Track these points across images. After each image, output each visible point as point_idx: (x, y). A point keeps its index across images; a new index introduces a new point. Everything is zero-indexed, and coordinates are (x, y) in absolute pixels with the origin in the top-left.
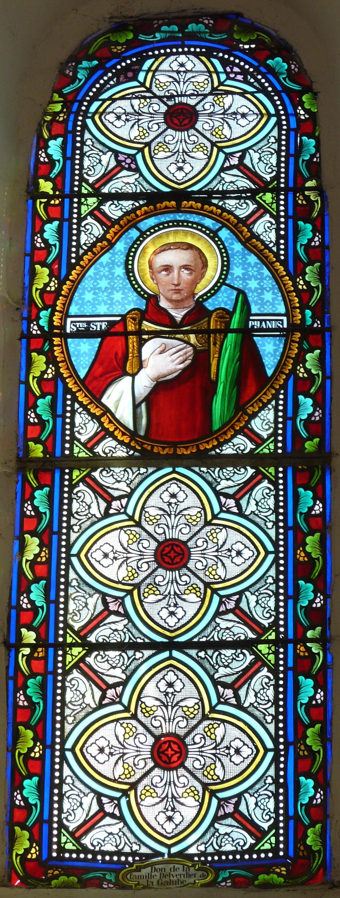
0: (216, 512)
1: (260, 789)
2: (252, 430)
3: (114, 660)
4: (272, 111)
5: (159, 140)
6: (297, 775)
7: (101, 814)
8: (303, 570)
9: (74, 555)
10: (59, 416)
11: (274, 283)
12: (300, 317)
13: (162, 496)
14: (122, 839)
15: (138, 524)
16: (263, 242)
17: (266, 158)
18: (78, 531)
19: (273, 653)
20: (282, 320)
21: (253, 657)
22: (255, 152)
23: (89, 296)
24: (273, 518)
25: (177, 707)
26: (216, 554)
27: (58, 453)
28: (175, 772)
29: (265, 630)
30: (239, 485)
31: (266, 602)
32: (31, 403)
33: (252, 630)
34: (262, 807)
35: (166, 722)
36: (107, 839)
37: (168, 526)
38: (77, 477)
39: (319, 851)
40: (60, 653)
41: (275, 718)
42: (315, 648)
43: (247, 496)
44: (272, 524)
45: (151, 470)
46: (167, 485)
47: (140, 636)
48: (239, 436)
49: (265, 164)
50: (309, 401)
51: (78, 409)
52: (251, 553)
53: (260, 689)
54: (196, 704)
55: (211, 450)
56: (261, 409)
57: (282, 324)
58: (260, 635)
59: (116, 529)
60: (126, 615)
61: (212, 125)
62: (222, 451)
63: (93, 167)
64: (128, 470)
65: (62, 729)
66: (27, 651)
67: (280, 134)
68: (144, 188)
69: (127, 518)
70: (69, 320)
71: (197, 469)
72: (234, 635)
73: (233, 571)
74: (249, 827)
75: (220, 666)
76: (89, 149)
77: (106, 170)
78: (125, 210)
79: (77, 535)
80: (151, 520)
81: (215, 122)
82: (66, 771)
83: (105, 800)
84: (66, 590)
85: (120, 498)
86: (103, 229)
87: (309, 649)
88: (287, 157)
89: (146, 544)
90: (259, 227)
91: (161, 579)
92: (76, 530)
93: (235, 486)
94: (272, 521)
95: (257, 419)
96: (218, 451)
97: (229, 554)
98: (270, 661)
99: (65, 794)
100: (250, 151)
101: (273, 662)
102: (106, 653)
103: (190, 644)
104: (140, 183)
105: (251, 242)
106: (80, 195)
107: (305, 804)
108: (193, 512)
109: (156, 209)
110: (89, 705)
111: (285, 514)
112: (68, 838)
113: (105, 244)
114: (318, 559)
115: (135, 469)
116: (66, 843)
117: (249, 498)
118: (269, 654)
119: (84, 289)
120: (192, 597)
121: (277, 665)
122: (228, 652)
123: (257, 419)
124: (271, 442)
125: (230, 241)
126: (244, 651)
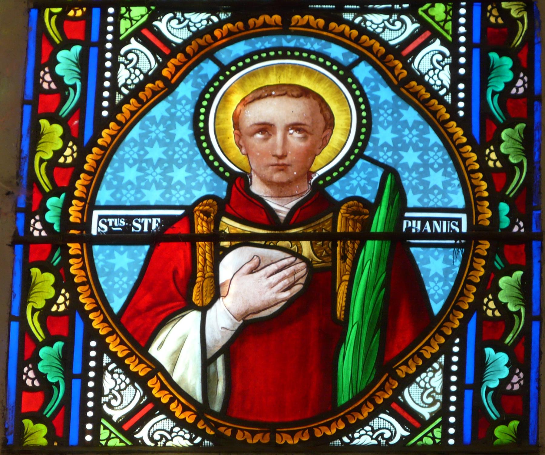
2: (405, 406)
10: (77, 377)
11: (447, 157)
16: (428, 87)
20: (459, 220)
23: (130, 174)
38: (127, 30)
48: (382, 415)
56: (421, 370)
62: (352, 439)
86: (157, 60)
90: (422, 62)
95: (414, 386)
102: (187, 15)
109: (247, 27)
124: (437, 426)
125: (373, 84)
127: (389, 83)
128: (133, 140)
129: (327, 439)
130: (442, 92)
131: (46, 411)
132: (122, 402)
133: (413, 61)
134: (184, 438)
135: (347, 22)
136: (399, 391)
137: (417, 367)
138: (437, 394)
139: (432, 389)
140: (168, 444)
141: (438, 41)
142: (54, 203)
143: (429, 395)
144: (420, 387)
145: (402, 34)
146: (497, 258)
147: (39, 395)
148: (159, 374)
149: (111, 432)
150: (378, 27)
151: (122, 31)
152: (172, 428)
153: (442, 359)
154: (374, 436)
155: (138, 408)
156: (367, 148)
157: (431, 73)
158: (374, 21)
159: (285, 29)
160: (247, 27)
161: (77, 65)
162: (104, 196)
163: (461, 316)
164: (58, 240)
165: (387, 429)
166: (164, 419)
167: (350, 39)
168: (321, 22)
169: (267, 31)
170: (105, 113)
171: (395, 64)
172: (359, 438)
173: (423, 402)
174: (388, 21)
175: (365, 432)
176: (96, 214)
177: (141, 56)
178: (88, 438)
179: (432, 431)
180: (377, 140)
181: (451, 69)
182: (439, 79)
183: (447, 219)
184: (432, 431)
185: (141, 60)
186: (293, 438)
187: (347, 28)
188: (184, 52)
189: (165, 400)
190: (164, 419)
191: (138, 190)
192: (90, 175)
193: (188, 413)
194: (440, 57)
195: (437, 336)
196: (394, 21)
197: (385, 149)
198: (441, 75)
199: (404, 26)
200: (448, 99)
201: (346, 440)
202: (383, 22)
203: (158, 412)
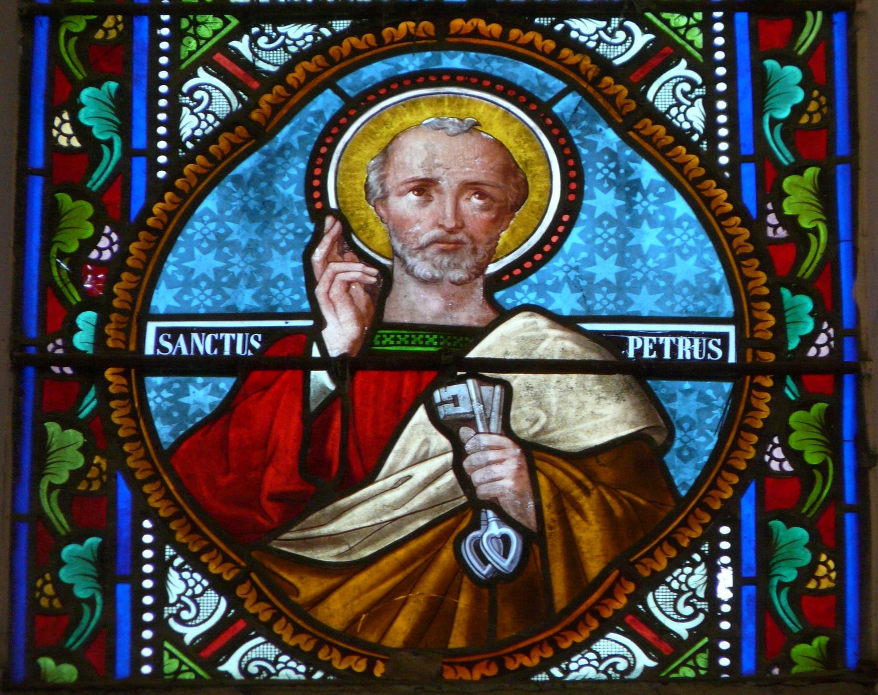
11: (703, 237)
12: (772, 320)
16: (672, 130)
19: (699, 24)
20: (724, 337)
21: (651, 36)
23: (205, 263)
32: (45, 552)
48: (611, 635)
50: (794, 73)
51: (173, 558)
56: (675, 564)
57: (725, 347)
62: (567, 672)
70: (151, 328)
86: (239, 99)
90: (661, 94)
95: (663, 588)
96: (556, 672)
98: (691, 43)
105: (640, 125)
107: (785, 121)
109: (380, 41)
113: (248, 130)
118: (688, 27)
119: (191, 244)
121: (709, 48)
123: (662, 592)
124: (702, 650)
125: (584, 255)
127: (611, 124)
129: (526, 673)
130: (178, 561)
131: (71, 641)
132: (197, 614)
133: (228, 611)
134: (578, 31)
135: (540, 29)
136: (248, 108)
137: (670, 560)
138: (700, 599)
139: (196, 111)
140: (603, 24)
142: (87, 319)
143: (199, 102)
144: (672, 590)
145: (627, 50)
148: (254, 576)
149: (182, 663)
150: (589, 40)
151: (184, 53)
152: (277, 657)
153: (705, 548)
154: (282, 37)
156: (577, 222)
157: (198, 590)
158: (583, 31)
159: (443, 42)
160: (380, 41)
163: (150, 221)
165: (263, 49)
166: (263, 643)
169: (411, 45)
171: (621, 96)
172: (305, 35)
173: (678, 613)
174: (605, 30)
175: (586, 662)
177: (215, 94)
178: (146, 669)
179: (693, 657)
180: (593, 209)
181: (705, 104)
182: (686, 120)
183: (699, 334)
184: (693, 657)
185: (211, 99)
186: (471, 671)
188: (602, 621)
189: (265, 617)
190: (263, 643)
192: (747, 425)
194: (687, 87)
195: (187, 190)
196: (614, 31)
197: (605, 223)
198: (181, 587)
199: (243, 666)
200: (169, 551)
201: (326, 32)
202: (597, 32)
203: (253, 633)
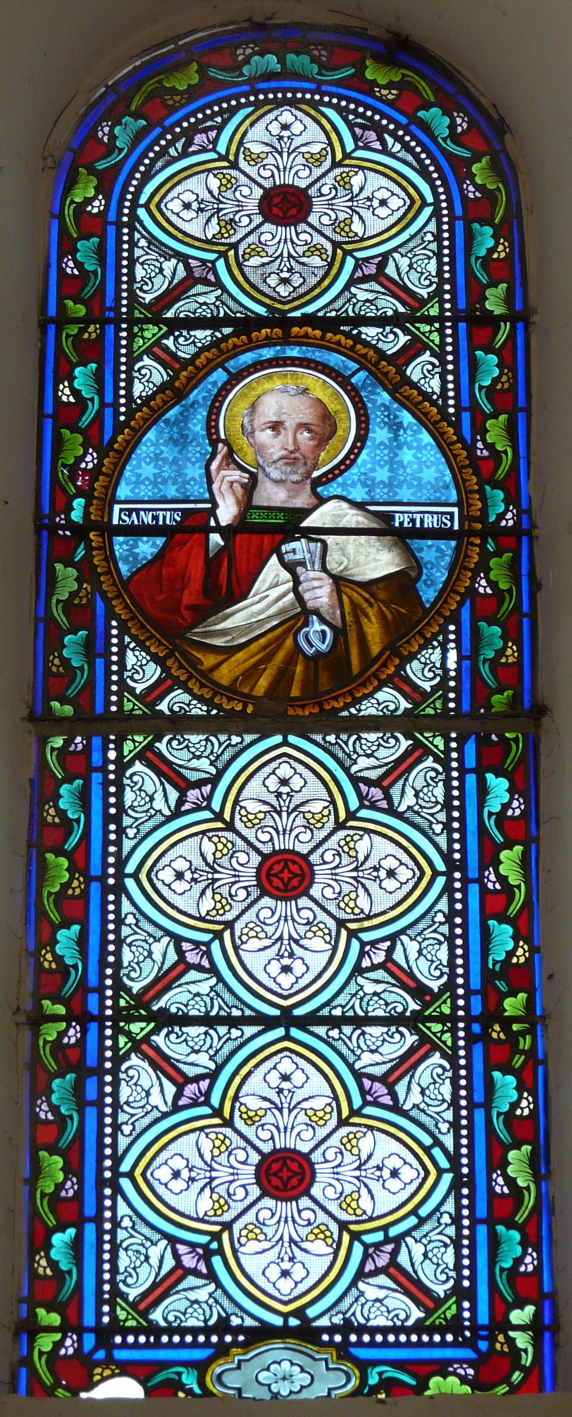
0: (352, 809)
1: (425, 929)
2: (408, 680)
3: (196, 1040)
4: (430, 199)
5: (250, 239)
6: (488, 1069)
7: (182, 967)
8: (495, 905)
9: (129, 876)
10: (91, 1104)
13: (267, 783)
14: (214, 1310)
15: (230, 827)
16: (421, 392)
17: (420, 264)
18: (135, 837)
19: (437, 330)
20: (451, 514)
22: (402, 256)
23: (148, 471)
24: (442, 817)
25: (295, 814)
26: (354, 874)
27: (99, 708)
28: (294, 1203)
29: (423, 302)
30: (386, 764)
31: (433, 952)
33: (403, 303)
34: (435, 1260)
35: (279, 1132)
36: (190, 1310)
37: (277, 830)
38: (130, 752)
39: (509, 591)
40: (106, 1319)
41: (447, 826)
42: (522, 1340)
43: (407, 1078)
44: (441, 826)
45: (248, 738)
46: (274, 765)
47: (241, 309)
49: (419, 272)
52: (411, 874)
53: (430, 1086)
54: (325, 808)
55: (342, 709)
58: (414, 310)
59: (196, 834)
60: (213, 970)
61: (334, 217)
62: (359, 711)
63: (150, 279)
64: (212, 738)
65: (114, 1145)
66: (74, 330)
67: (459, 1207)
68: (224, 1310)
69: (212, 816)
71: (318, 738)
72: (378, 310)
73: (383, 901)
74: (414, 1290)
75: (359, 756)
76: (130, 931)
77: (160, 969)
78: (199, 345)
79: (133, 843)
80: (250, 821)
81: (346, 1185)
82: (122, 1209)
83: (186, 946)
84: (117, 932)
85: (197, 1079)
87: (511, 1342)
88: (471, 1108)
89: (246, 191)
90: (414, 371)
91: (268, 236)
92: (131, 835)
93: (380, 766)
94: (448, 1122)
95: (415, 661)
97: (375, 874)
99: (120, 1245)
100: (403, 937)
101: (449, 1043)
102: (184, 1029)
103: (313, 1019)
104: (223, 303)
106: (132, 322)
108: (316, 807)
109: (250, 340)
110: (160, 811)
111: (462, 809)
112: (134, 704)
113: (173, 392)
114: (519, 887)
115: (223, 738)
116: (134, 741)
117: (410, 1082)
120: (319, 1247)
122: (376, 1031)
123: (415, 664)
124: (438, 698)
125: (369, 466)
126: (402, 1029)
127: (385, 389)
128: (149, 440)
135: (343, 333)
141: (438, 1054)
146: (490, 540)
147: (54, 1127)
153: (441, 638)
155: (159, 681)
160: (250, 340)
161: (72, 1249)
162: (123, 492)
164: (80, 532)
167: (345, 348)
168: (318, 333)
170: (122, 418)
176: (117, 508)
178: (114, 709)
184: (433, 702)
187: (343, 338)
191: (155, 484)
193: (206, 690)
194: (440, 1071)
